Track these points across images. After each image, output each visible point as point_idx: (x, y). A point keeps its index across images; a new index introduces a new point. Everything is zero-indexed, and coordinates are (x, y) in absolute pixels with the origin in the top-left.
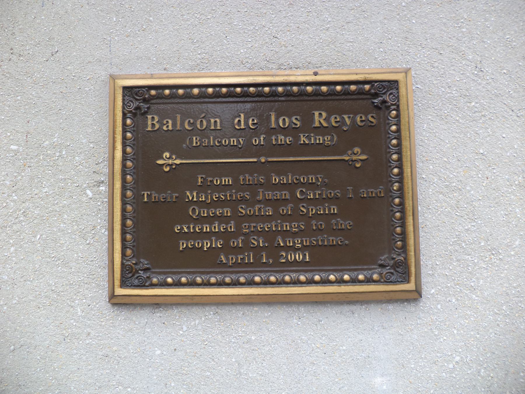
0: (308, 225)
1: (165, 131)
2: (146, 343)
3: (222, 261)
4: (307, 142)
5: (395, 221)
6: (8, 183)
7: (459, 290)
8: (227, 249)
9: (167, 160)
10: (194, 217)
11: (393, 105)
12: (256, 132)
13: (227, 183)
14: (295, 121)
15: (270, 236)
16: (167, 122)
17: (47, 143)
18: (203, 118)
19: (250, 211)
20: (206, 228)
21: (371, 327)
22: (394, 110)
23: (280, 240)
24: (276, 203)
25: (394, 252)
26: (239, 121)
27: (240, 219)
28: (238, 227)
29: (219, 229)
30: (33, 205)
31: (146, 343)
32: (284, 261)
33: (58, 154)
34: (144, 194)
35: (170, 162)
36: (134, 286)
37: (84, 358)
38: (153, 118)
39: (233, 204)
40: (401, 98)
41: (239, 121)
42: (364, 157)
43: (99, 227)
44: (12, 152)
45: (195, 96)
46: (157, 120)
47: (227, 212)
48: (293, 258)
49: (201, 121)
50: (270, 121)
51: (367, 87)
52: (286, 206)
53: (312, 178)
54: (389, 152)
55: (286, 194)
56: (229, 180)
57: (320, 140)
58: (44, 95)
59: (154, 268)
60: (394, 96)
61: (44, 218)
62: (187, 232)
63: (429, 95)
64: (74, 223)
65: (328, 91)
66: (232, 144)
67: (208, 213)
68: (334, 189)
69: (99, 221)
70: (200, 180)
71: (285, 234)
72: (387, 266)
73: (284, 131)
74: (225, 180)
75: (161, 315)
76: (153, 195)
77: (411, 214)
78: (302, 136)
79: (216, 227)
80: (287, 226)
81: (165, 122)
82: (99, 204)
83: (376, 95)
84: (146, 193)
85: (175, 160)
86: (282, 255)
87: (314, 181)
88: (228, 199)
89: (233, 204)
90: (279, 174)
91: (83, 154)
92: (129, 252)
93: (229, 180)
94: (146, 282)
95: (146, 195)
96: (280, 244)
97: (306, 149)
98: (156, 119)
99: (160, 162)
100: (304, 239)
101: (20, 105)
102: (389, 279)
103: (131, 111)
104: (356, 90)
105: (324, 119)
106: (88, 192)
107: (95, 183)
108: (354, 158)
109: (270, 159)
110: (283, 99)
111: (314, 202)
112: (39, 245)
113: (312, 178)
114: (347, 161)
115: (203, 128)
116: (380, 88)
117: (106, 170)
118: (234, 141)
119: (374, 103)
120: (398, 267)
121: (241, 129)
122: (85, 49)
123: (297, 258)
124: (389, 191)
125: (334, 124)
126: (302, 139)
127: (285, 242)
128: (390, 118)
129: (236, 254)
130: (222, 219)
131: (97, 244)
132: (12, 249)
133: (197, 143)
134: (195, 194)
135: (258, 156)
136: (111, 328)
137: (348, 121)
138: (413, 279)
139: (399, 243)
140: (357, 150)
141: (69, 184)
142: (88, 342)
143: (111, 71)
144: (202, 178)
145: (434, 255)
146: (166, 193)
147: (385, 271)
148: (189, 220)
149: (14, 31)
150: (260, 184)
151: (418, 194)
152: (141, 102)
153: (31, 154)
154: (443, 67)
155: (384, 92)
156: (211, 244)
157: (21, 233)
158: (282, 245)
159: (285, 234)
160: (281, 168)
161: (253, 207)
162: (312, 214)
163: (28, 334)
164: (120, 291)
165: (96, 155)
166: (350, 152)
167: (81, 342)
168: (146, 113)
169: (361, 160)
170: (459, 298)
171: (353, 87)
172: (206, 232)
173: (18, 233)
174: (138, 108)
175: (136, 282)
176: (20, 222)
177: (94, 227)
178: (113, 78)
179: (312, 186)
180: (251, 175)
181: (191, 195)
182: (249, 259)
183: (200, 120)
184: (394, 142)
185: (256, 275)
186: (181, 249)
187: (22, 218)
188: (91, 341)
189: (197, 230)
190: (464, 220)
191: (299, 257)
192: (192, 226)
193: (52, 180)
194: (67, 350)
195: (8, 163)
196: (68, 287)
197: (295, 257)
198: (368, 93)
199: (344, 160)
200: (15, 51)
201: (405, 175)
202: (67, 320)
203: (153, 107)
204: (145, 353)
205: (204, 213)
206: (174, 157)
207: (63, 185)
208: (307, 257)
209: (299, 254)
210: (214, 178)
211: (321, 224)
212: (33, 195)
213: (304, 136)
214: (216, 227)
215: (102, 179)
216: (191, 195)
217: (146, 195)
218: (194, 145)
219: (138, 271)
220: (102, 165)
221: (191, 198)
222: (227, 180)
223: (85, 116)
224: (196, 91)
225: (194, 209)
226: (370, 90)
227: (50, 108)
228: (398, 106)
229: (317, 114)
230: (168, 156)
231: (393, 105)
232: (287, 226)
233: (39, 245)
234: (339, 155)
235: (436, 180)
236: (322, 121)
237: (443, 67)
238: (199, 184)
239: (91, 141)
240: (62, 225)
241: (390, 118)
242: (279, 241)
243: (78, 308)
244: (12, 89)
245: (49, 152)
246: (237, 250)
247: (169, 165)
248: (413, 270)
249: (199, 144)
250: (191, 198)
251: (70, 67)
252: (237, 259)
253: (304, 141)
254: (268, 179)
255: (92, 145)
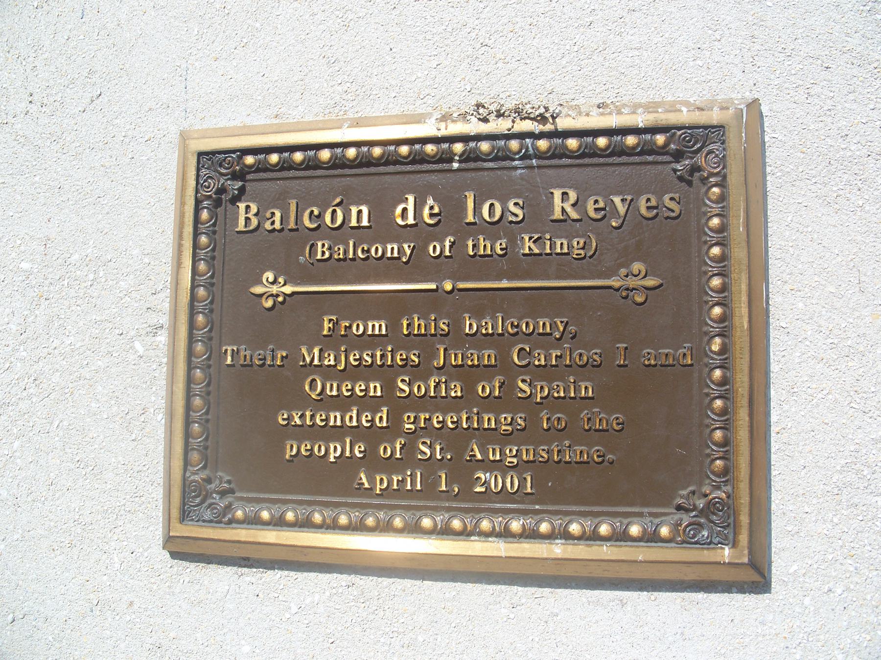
0: (533, 420)
1: (269, 231)
2: (225, 630)
3: (363, 484)
4: (536, 251)
5: (713, 416)
6: (12, 326)
7: (852, 569)
8: (372, 462)
9: (271, 286)
10: (314, 397)
11: (712, 175)
12: (435, 231)
13: (377, 332)
14: (512, 208)
15: (455, 440)
16: (273, 214)
17: (76, 257)
18: (337, 205)
19: (418, 389)
20: (335, 418)
21: (658, 634)
22: (716, 185)
23: (475, 447)
24: (468, 375)
25: (707, 481)
26: (405, 210)
27: (398, 406)
28: (395, 418)
29: (359, 420)
30: (50, 367)
31: (225, 630)
32: (483, 490)
33: (91, 277)
34: (226, 350)
35: (274, 289)
36: (204, 521)
37: (122, 646)
38: (248, 207)
39: (386, 373)
40: (730, 161)
41: (405, 210)
42: (651, 282)
43: (152, 410)
44: (22, 274)
45: (324, 163)
46: (256, 210)
47: (376, 389)
48: (500, 485)
49: (334, 211)
50: (465, 209)
51: (660, 139)
52: (490, 380)
53: (543, 324)
54: (705, 273)
55: (489, 356)
56: (380, 326)
57: (561, 245)
58: (76, 172)
59: (241, 490)
60: (717, 156)
61: (67, 391)
62: (299, 426)
63: (799, 154)
64: (113, 402)
65: (580, 147)
66: (354, 223)
67: (339, 388)
68: (588, 347)
69: (153, 398)
70: (326, 325)
71: (488, 436)
72: (692, 510)
73: (494, 228)
74: (373, 326)
75: (253, 580)
76: (242, 353)
77: (745, 402)
78: (527, 239)
79: (352, 418)
80: (489, 421)
81: (268, 215)
82: (154, 367)
83: (678, 156)
84: (229, 348)
85: (285, 285)
86: (478, 478)
87: (548, 330)
88: (379, 363)
89: (386, 373)
90: (478, 314)
91: (132, 276)
92: (195, 456)
93: (380, 326)
94: (224, 516)
95: (229, 352)
96: (474, 456)
97: (536, 264)
98: (254, 208)
99: (258, 290)
100: (524, 448)
101: (39, 190)
102: (693, 537)
103: (210, 196)
104: (638, 145)
105: (573, 205)
106: (138, 345)
107: (149, 329)
108: (632, 282)
109: (461, 285)
110: (491, 165)
111: (546, 373)
112: (57, 439)
113: (543, 324)
114: (617, 290)
115: (337, 225)
116: (689, 141)
117: (166, 306)
118: (392, 249)
119: (675, 171)
120: (714, 514)
121: (406, 226)
122: (144, 87)
123: (509, 485)
124: (700, 353)
125: (592, 214)
126: (527, 244)
127: (484, 452)
128: (708, 202)
129: (389, 474)
130: (367, 403)
131: (148, 441)
132: (17, 444)
133: (323, 253)
134: (316, 351)
135: (440, 280)
136: (168, 597)
137: (622, 209)
138: (744, 538)
139: (718, 462)
140: (637, 267)
141: (107, 330)
142: (128, 618)
143: (185, 125)
144: (330, 320)
145: (801, 492)
146: (265, 349)
147: (686, 519)
148: (302, 402)
149: (36, 63)
150: (441, 335)
151: (772, 361)
152: (228, 179)
153: (50, 276)
154: (832, 94)
155: (695, 147)
156: (343, 451)
157: (30, 416)
158: (479, 457)
159: (488, 436)
160: (484, 303)
161: (426, 380)
162: (541, 398)
163: (36, 595)
164: (180, 530)
165: (153, 278)
166: (623, 271)
167: (117, 618)
168: (235, 200)
169: (646, 288)
170: (852, 587)
171: (631, 140)
172: (335, 427)
173: (26, 416)
174: (222, 191)
175: (208, 515)
176: (30, 397)
177: (144, 411)
178: (184, 137)
179: (544, 340)
180: (424, 316)
181: (312, 355)
182: (413, 483)
183: (330, 210)
184: (716, 251)
185: (426, 515)
186: (287, 457)
187: (31, 391)
188: (133, 616)
189: (318, 421)
190: (870, 421)
191: (512, 483)
192: (308, 414)
193: (81, 324)
194: (96, 629)
195: (16, 293)
196: (100, 517)
197: (504, 483)
198: (662, 150)
199: (610, 287)
200: (35, 97)
201: (736, 320)
202: (96, 576)
203: (249, 187)
204: (224, 647)
205: (331, 390)
206: (281, 280)
207: (97, 331)
208: (529, 485)
209: (512, 477)
210: (353, 321)
211: (559, 419)
212: (50, 350)
213: (530, 238)
214: (352, 418)
215: (161, 322)
216: (312, 355)
217: (229, 352)
218: (319, 257)
219: (212, 493)
220: (162, 295)
221: (308, 360)
222: (377, 327)
223: (139, 207)
224: (325, 155)
225: (314, 380)
226: (666, 144)
227: (84, 195)
228: (725, 177)
229: (557, 194)
230: (271, 279)
231: (712, 175)
232: (489, 421)
233: (57, 439)
234: (599, 277)
235: (809, 333)
236: (569, 209)
237: (832, 94)
238: (325, 333)
239: (146, 252)
240: (93, 405)
241: (708, 202)
242: (472, 450)
243: (115, 555)
244: (27, 163)
245: (78, 273)
246: (390, 465)
247: (272, 295)
248: (744, 519)
249: (327, 255)
250: (308, 360)
251: (118, 121)
252: (390, 482)
253: (530, 248)
254: (456, 324)
255: (146, 260)
